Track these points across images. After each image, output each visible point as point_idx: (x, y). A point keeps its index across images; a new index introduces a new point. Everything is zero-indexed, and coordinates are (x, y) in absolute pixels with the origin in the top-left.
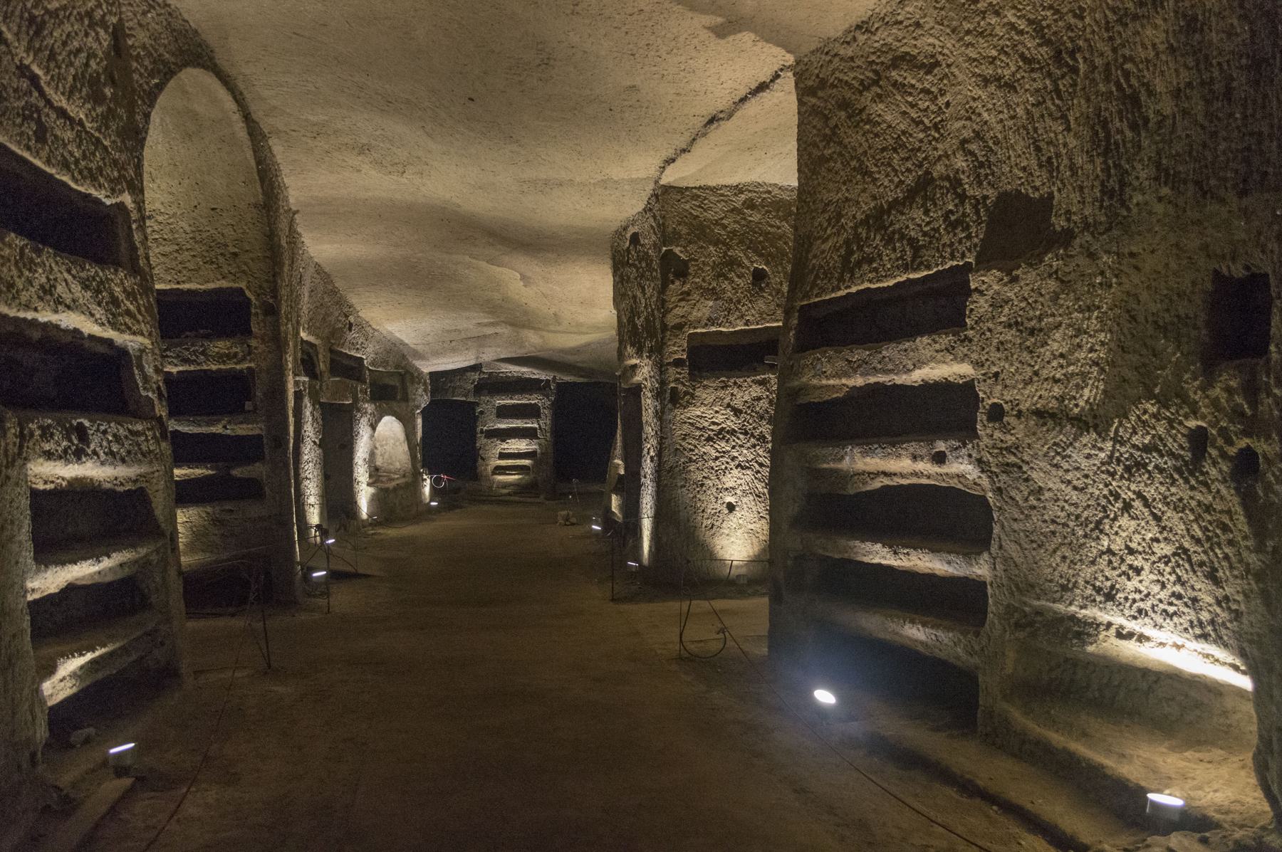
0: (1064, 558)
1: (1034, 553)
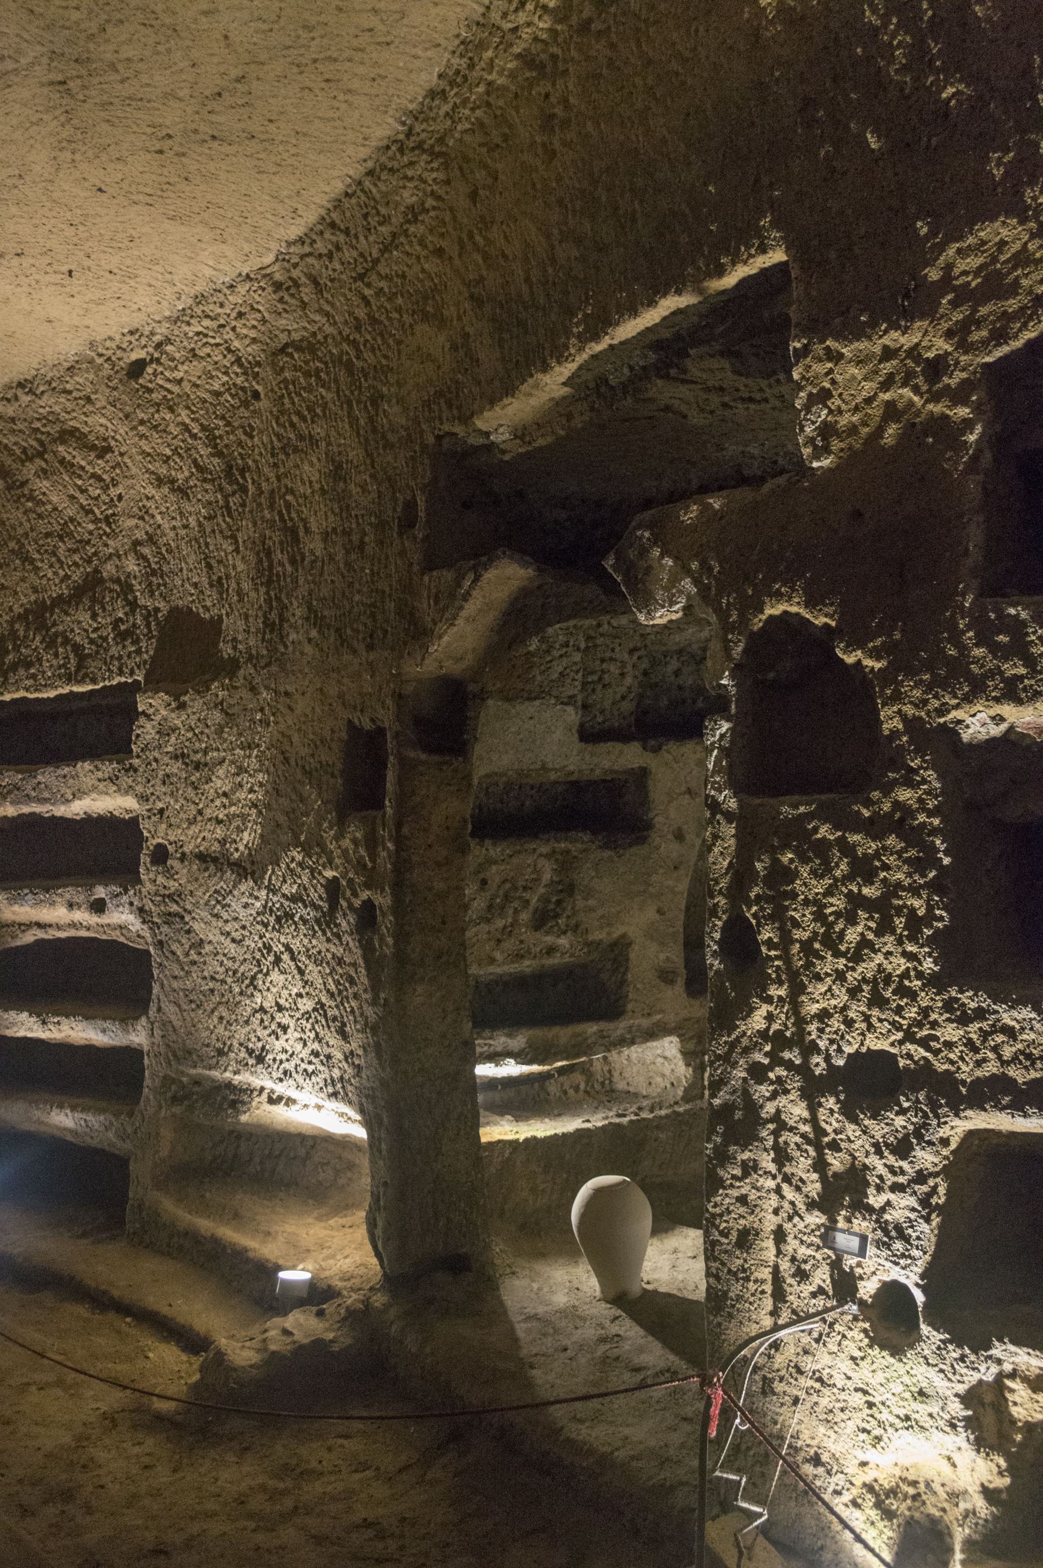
0: (221, 1018)
1: (193, 1015)
